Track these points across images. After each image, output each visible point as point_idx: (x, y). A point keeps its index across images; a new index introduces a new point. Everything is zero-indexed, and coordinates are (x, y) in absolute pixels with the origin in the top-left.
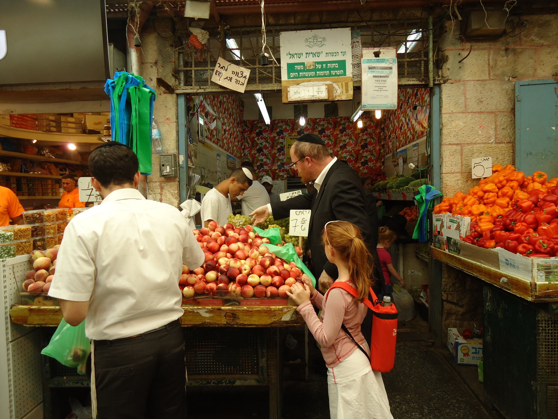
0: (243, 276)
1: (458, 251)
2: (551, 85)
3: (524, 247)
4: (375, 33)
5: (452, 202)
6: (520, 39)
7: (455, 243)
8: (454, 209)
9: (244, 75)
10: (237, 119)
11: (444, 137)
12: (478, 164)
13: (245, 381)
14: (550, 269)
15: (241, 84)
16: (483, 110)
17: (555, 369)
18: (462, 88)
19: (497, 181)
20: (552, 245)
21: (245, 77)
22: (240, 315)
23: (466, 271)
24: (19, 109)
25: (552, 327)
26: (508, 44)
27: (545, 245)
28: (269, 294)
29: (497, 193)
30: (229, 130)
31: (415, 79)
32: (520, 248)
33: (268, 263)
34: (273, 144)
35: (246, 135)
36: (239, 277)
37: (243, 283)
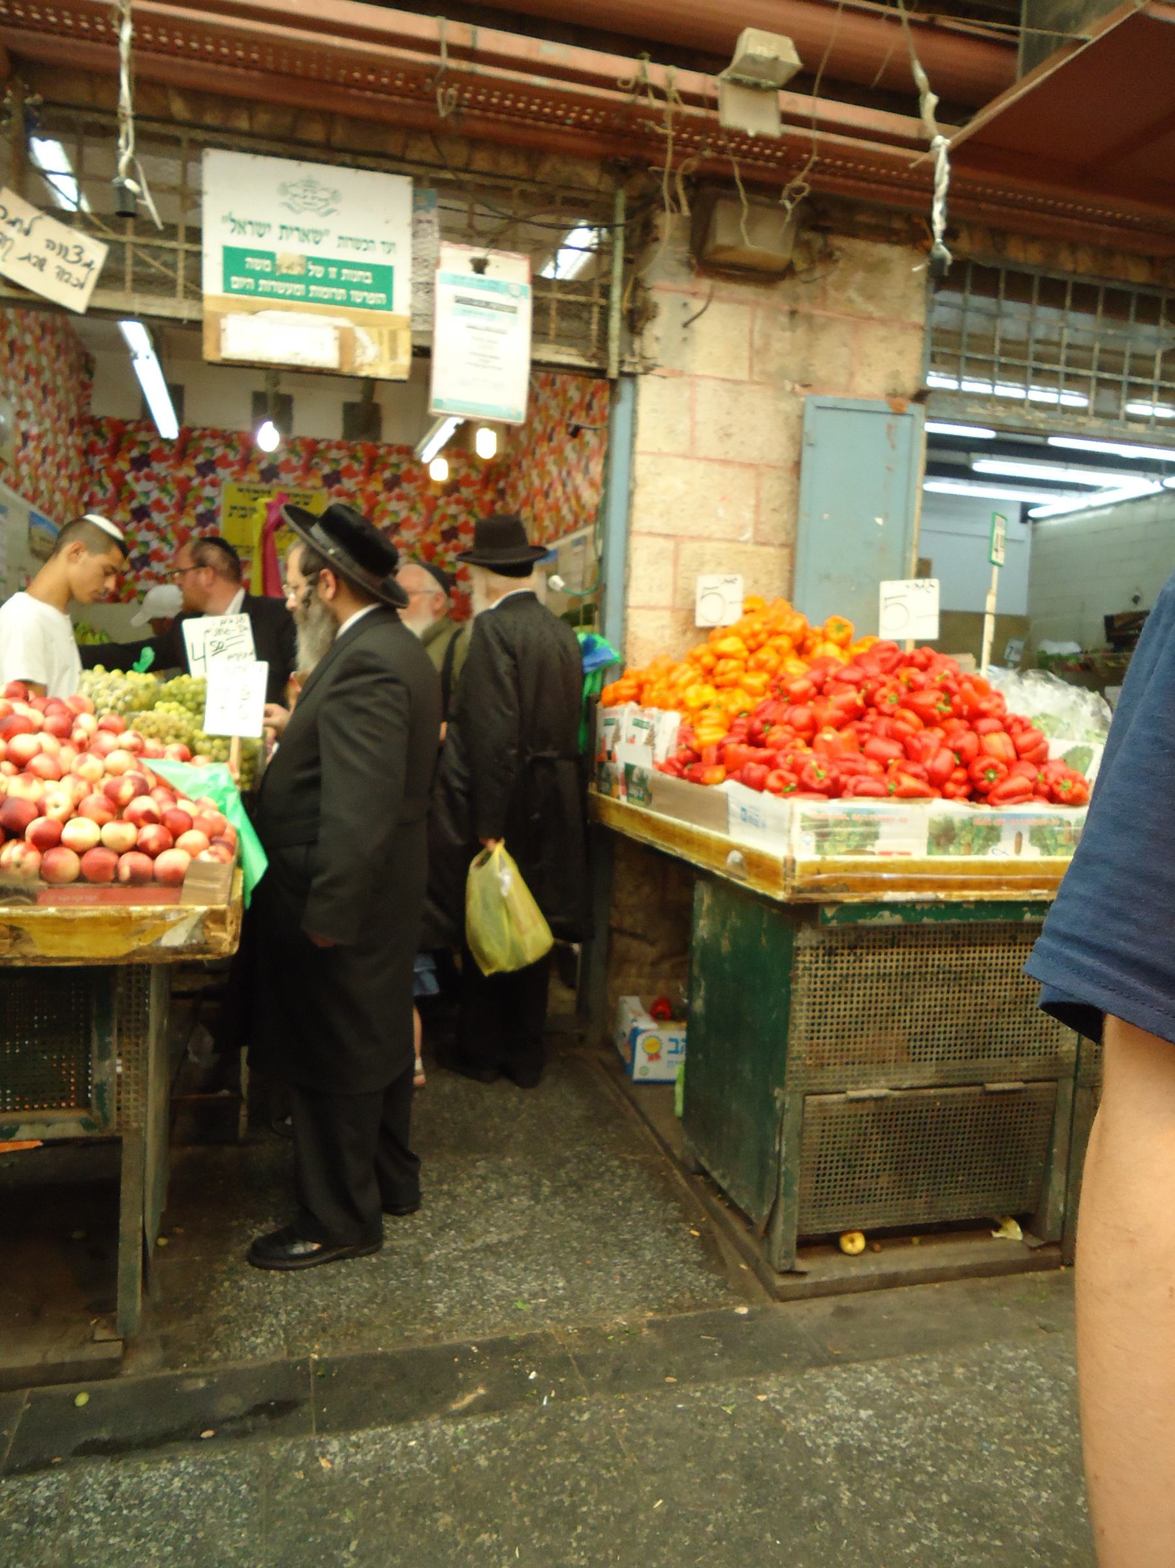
0: (50, 822)
1: (647, 798)
2: (881, 416)
3: (781, 778)
4: (479, 209)
5: (643, 677)
6: (824, 291)
7: (642, 781)
8: (645, 696)
9: (87, 258)
10: (68, 409)
11: (637, 514)
12: (712, 591)
13: (48, 1125)
14: (826, 826)
16: (731, 455)
17: (823, 1058)
18: (687, 394)
19: (746, 631)
20: (835, 773)
21: (89, 265)
22: (35, 932)
23: (662, 845)
25: (823, 962)
26: (796, 298)
27: (822, 773)
28: (125, 872)
29: (746, 661)
30: (40, 437)
31: (573, 351)
32: (772, 780)
33: (127, 790)
34: (184, 498)
35: (97, 462)
36: (34, 826)
37: (48, 842)
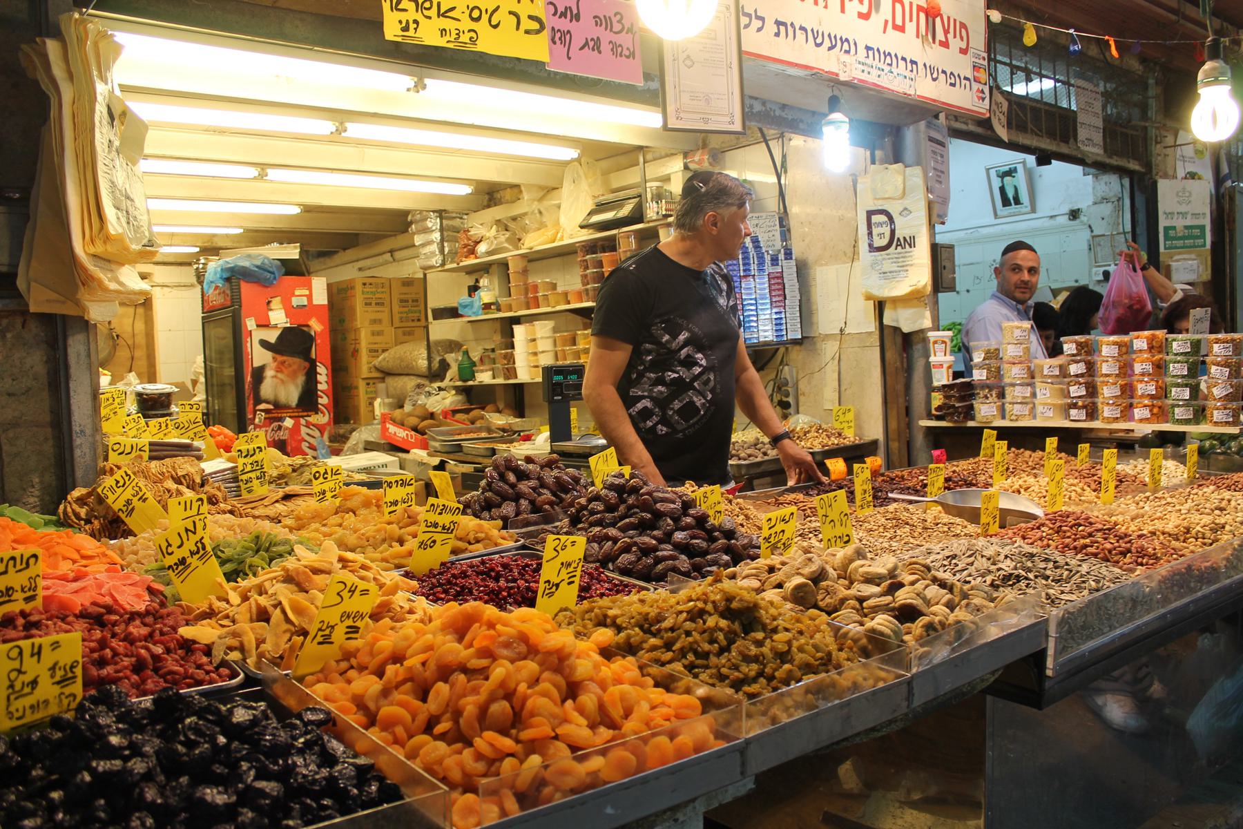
15: (627, 53)
24: (360, 264)
